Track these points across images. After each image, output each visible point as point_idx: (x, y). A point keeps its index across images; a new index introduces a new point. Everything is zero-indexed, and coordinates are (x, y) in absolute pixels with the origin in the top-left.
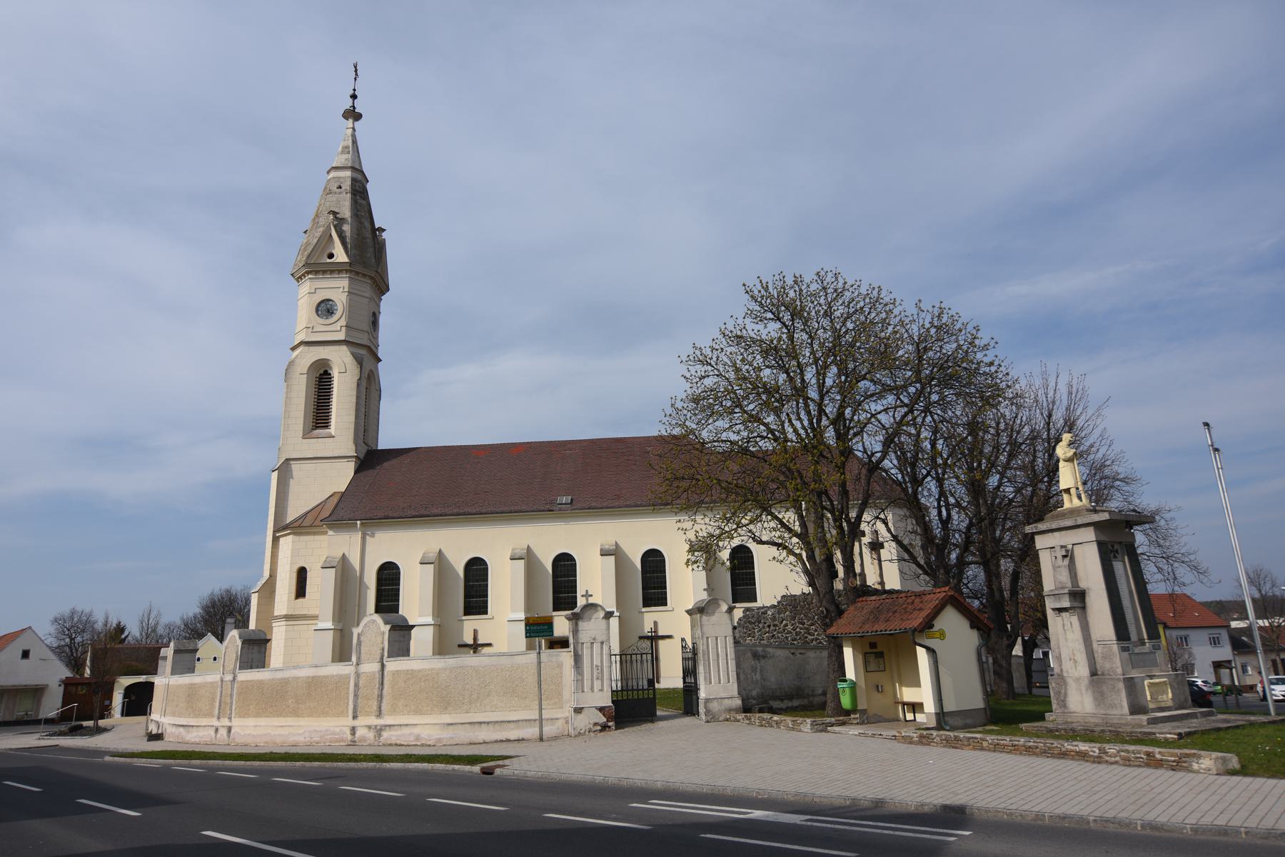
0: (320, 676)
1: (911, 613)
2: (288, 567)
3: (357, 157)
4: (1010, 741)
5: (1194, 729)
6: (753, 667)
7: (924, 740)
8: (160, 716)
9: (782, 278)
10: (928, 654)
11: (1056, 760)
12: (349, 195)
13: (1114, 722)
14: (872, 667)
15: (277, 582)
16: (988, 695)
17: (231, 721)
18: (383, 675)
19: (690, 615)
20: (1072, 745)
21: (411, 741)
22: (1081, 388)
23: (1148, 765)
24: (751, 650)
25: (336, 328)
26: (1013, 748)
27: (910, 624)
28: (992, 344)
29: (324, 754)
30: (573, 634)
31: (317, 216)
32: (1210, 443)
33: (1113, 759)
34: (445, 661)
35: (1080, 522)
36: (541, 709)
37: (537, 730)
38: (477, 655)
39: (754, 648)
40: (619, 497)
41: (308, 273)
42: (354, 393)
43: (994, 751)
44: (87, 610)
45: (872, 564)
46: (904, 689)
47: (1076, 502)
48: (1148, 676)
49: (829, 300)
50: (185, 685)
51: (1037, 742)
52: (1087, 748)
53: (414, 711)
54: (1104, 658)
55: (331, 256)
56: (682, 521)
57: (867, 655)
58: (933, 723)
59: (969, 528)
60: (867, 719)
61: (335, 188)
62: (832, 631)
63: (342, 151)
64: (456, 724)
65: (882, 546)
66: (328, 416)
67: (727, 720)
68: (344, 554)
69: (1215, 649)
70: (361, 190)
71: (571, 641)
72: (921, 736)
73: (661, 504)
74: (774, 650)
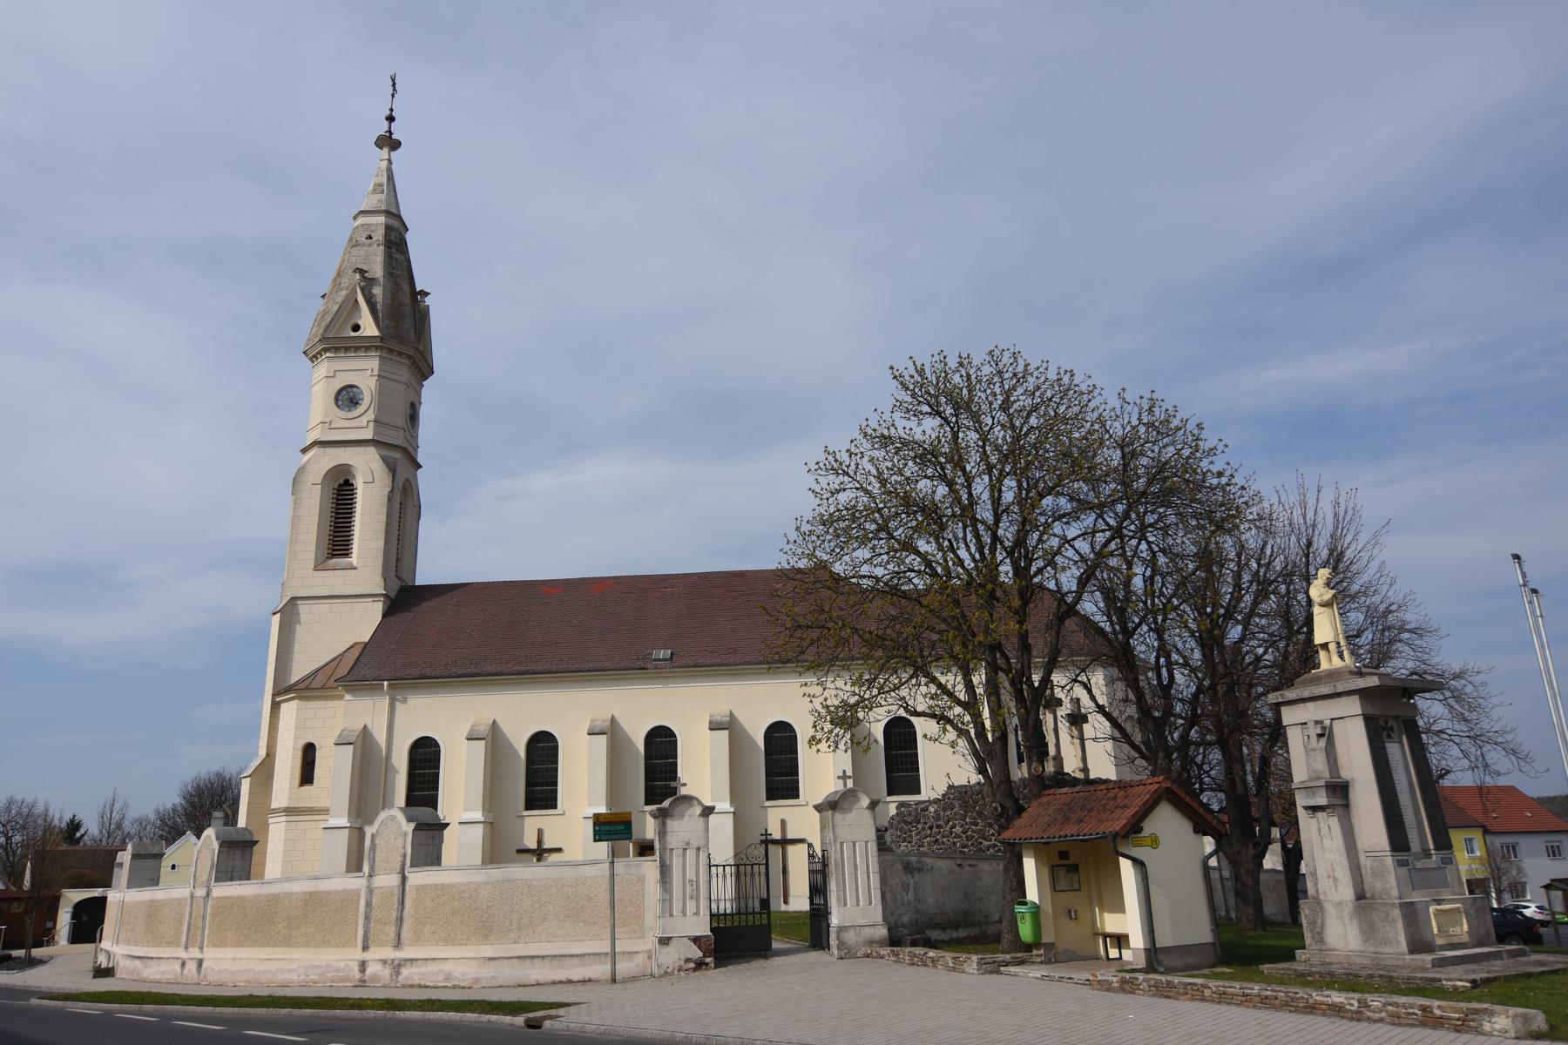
0: (320, 892)
1: (1112, 812)
2: (290, 743)
3: (393, 199)
4: (1241, 988)
5: (1494, 975)
6: (903, 883)
7: (1127, 987)
8: (113, 945)
9: (942, 359)
10: (1134, 868)
11: (1301, 1016)
12: (382, 248)
13: (1387, 963)
14: (1063, 885)
15: (276, 764)
16: (1218, 923)
17: (202, 952)
18: (404, 890)
19: (819, 811)
20: (1322, 996)
21: (439, 980)
22: (1351, 506)
23: (1423, 1024)
24: (901, 860)
25: (362, 424)
26: (1244, 999)
27: (1110, 826)
28: (1220, 448)
29: (320, 998)
30: (659, 836)
31: (339, 275)
32: (1521, 582)
33: (1377, 1015)
34: (487, 873)
35: (1340, 689)
36: (613, 940)
37: (608, 967)
38: (541, 863)
39: (906, 858)
40: (735, 651)
41: (326, 350)
42: (384, 510)
43: (1219, 1002)
44: (30, 799)
45: (1072, 743)
46: (1107, 916)
47: (1337, 662)
48: (1435, 900)
49: (1007, 387)
50: (145, 902)
51: (1276, 991)
52: (1342, 1000)
53: (444, 940)
54: (1374, 875)
55: (356, 328)
56: (809, 683)
57: (1055, 868)
58: (1142, 963)
59: (1196, 696)
60: (1056, 956)
61: (364, 239)
62: (1008, 834)
63: (374, 190)
64: (499, 958)
65: (1085, 719)
66: (349, 541)
67: (868, 956)
68: (365, 726)
69: (1554, 863)
70: (399, 242)
71: (657, 846)
72: (1123, 981)
73: (777, 662)
74: (934, 860)
